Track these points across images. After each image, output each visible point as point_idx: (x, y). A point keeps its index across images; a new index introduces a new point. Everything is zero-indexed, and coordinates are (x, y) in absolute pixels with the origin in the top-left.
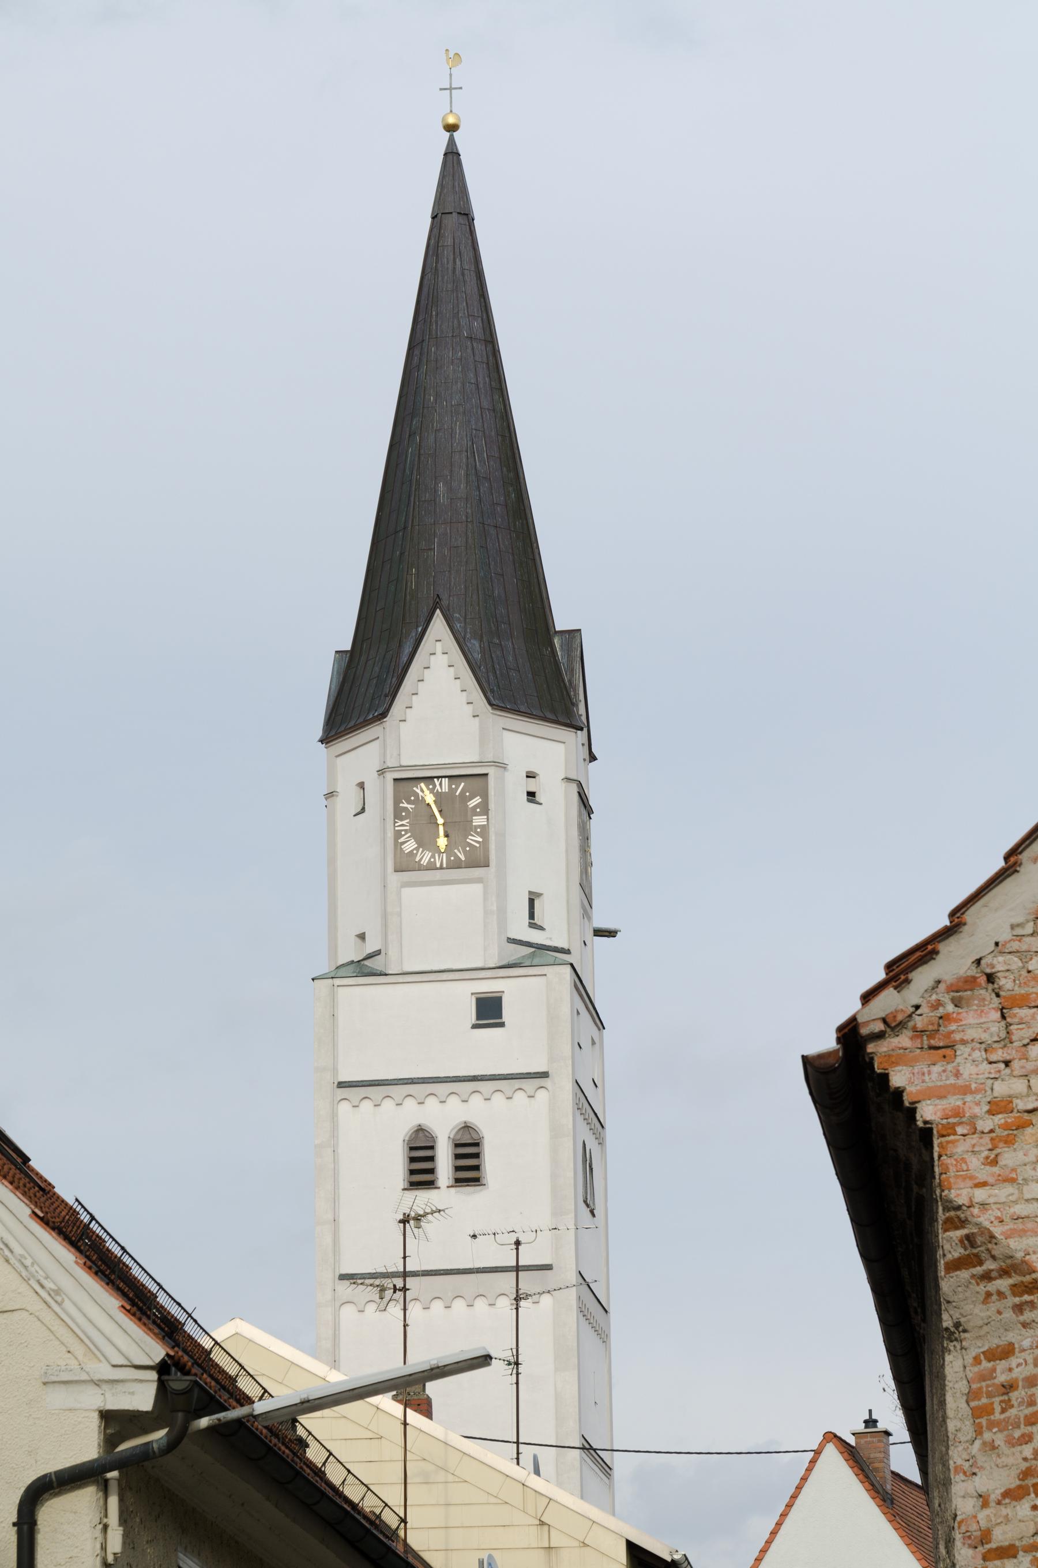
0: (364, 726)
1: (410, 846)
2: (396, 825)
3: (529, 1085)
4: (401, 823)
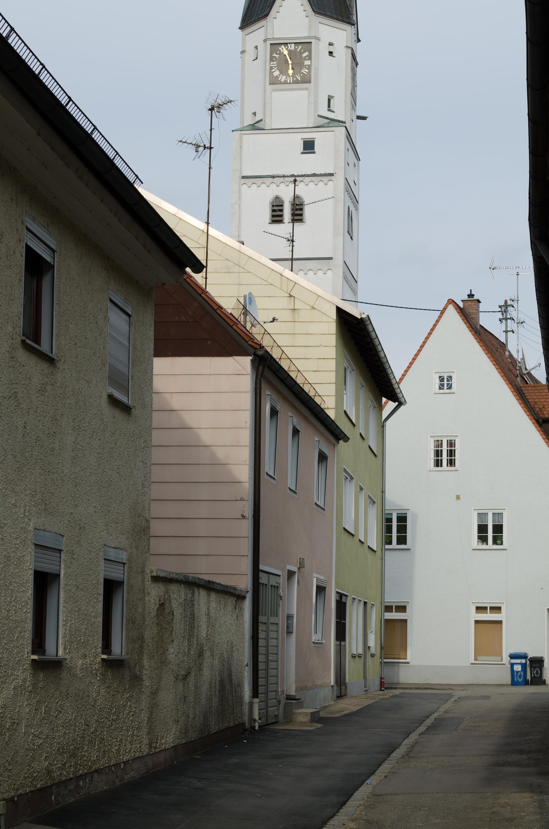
0: (258, 21)
1: (277, 73)
2: (271, 64)
3: (325, 179)
4: (273, 63)
